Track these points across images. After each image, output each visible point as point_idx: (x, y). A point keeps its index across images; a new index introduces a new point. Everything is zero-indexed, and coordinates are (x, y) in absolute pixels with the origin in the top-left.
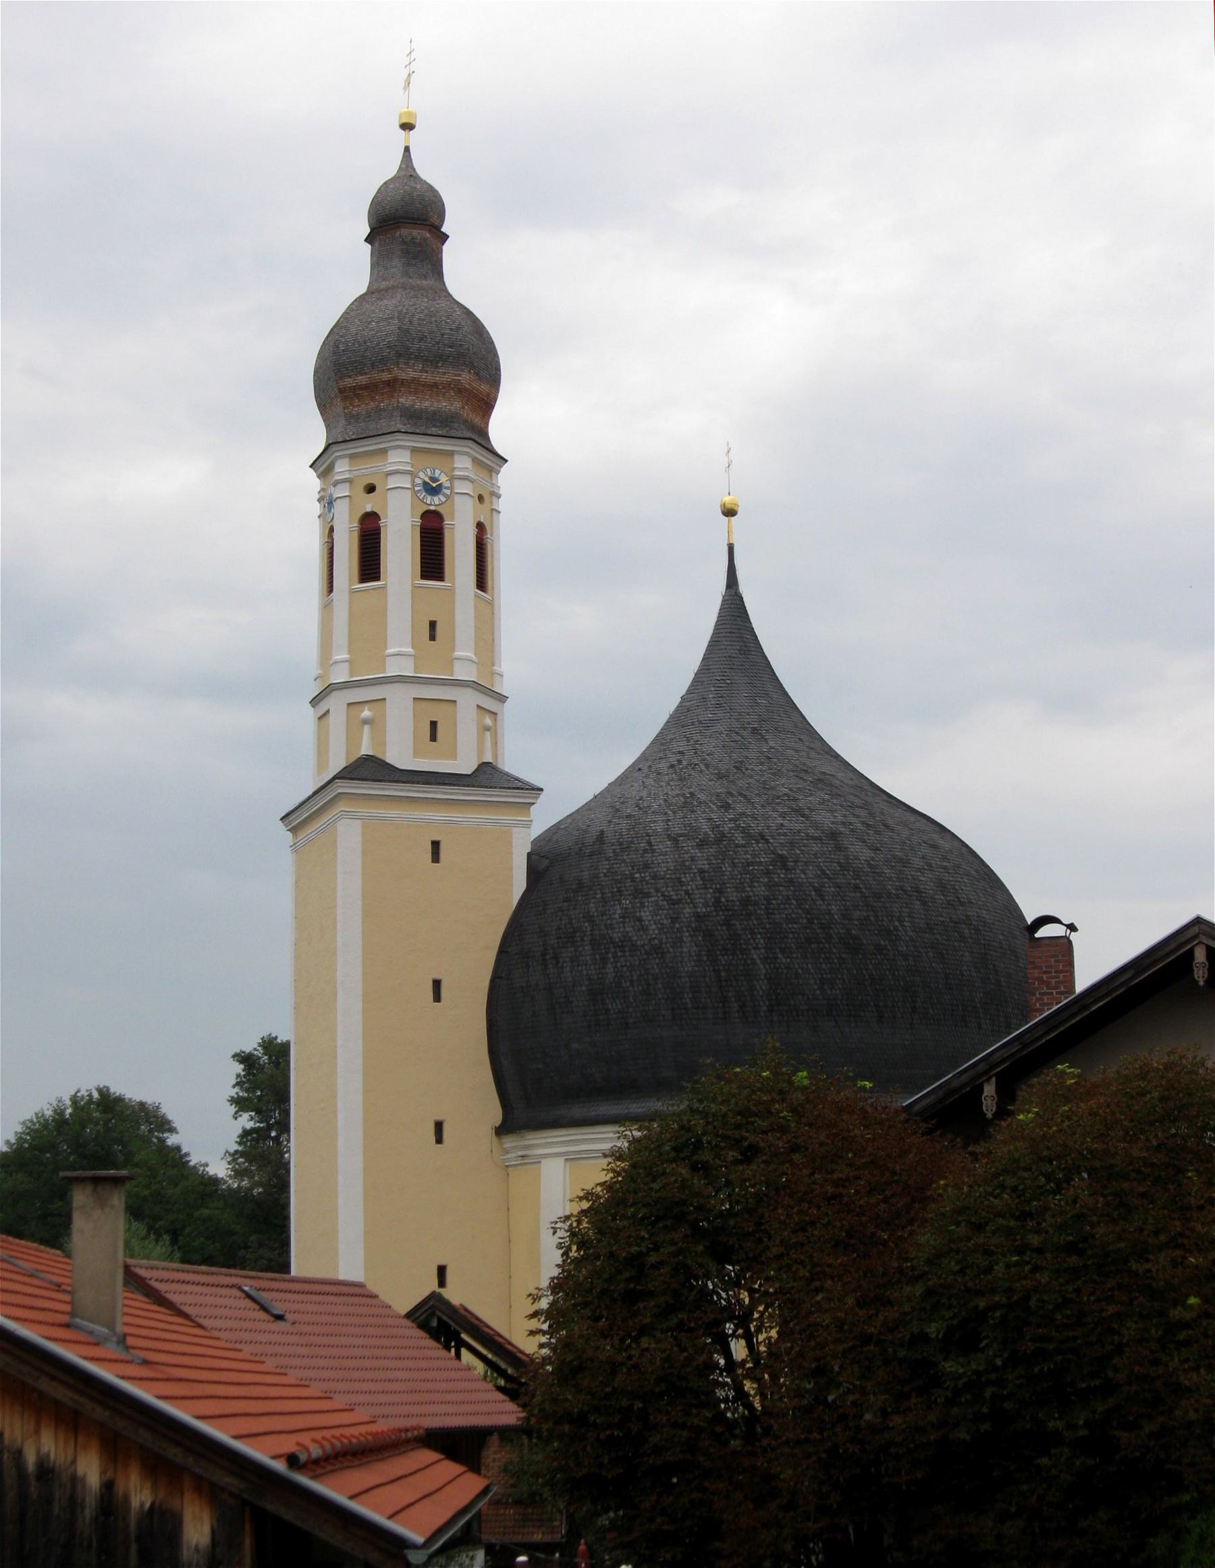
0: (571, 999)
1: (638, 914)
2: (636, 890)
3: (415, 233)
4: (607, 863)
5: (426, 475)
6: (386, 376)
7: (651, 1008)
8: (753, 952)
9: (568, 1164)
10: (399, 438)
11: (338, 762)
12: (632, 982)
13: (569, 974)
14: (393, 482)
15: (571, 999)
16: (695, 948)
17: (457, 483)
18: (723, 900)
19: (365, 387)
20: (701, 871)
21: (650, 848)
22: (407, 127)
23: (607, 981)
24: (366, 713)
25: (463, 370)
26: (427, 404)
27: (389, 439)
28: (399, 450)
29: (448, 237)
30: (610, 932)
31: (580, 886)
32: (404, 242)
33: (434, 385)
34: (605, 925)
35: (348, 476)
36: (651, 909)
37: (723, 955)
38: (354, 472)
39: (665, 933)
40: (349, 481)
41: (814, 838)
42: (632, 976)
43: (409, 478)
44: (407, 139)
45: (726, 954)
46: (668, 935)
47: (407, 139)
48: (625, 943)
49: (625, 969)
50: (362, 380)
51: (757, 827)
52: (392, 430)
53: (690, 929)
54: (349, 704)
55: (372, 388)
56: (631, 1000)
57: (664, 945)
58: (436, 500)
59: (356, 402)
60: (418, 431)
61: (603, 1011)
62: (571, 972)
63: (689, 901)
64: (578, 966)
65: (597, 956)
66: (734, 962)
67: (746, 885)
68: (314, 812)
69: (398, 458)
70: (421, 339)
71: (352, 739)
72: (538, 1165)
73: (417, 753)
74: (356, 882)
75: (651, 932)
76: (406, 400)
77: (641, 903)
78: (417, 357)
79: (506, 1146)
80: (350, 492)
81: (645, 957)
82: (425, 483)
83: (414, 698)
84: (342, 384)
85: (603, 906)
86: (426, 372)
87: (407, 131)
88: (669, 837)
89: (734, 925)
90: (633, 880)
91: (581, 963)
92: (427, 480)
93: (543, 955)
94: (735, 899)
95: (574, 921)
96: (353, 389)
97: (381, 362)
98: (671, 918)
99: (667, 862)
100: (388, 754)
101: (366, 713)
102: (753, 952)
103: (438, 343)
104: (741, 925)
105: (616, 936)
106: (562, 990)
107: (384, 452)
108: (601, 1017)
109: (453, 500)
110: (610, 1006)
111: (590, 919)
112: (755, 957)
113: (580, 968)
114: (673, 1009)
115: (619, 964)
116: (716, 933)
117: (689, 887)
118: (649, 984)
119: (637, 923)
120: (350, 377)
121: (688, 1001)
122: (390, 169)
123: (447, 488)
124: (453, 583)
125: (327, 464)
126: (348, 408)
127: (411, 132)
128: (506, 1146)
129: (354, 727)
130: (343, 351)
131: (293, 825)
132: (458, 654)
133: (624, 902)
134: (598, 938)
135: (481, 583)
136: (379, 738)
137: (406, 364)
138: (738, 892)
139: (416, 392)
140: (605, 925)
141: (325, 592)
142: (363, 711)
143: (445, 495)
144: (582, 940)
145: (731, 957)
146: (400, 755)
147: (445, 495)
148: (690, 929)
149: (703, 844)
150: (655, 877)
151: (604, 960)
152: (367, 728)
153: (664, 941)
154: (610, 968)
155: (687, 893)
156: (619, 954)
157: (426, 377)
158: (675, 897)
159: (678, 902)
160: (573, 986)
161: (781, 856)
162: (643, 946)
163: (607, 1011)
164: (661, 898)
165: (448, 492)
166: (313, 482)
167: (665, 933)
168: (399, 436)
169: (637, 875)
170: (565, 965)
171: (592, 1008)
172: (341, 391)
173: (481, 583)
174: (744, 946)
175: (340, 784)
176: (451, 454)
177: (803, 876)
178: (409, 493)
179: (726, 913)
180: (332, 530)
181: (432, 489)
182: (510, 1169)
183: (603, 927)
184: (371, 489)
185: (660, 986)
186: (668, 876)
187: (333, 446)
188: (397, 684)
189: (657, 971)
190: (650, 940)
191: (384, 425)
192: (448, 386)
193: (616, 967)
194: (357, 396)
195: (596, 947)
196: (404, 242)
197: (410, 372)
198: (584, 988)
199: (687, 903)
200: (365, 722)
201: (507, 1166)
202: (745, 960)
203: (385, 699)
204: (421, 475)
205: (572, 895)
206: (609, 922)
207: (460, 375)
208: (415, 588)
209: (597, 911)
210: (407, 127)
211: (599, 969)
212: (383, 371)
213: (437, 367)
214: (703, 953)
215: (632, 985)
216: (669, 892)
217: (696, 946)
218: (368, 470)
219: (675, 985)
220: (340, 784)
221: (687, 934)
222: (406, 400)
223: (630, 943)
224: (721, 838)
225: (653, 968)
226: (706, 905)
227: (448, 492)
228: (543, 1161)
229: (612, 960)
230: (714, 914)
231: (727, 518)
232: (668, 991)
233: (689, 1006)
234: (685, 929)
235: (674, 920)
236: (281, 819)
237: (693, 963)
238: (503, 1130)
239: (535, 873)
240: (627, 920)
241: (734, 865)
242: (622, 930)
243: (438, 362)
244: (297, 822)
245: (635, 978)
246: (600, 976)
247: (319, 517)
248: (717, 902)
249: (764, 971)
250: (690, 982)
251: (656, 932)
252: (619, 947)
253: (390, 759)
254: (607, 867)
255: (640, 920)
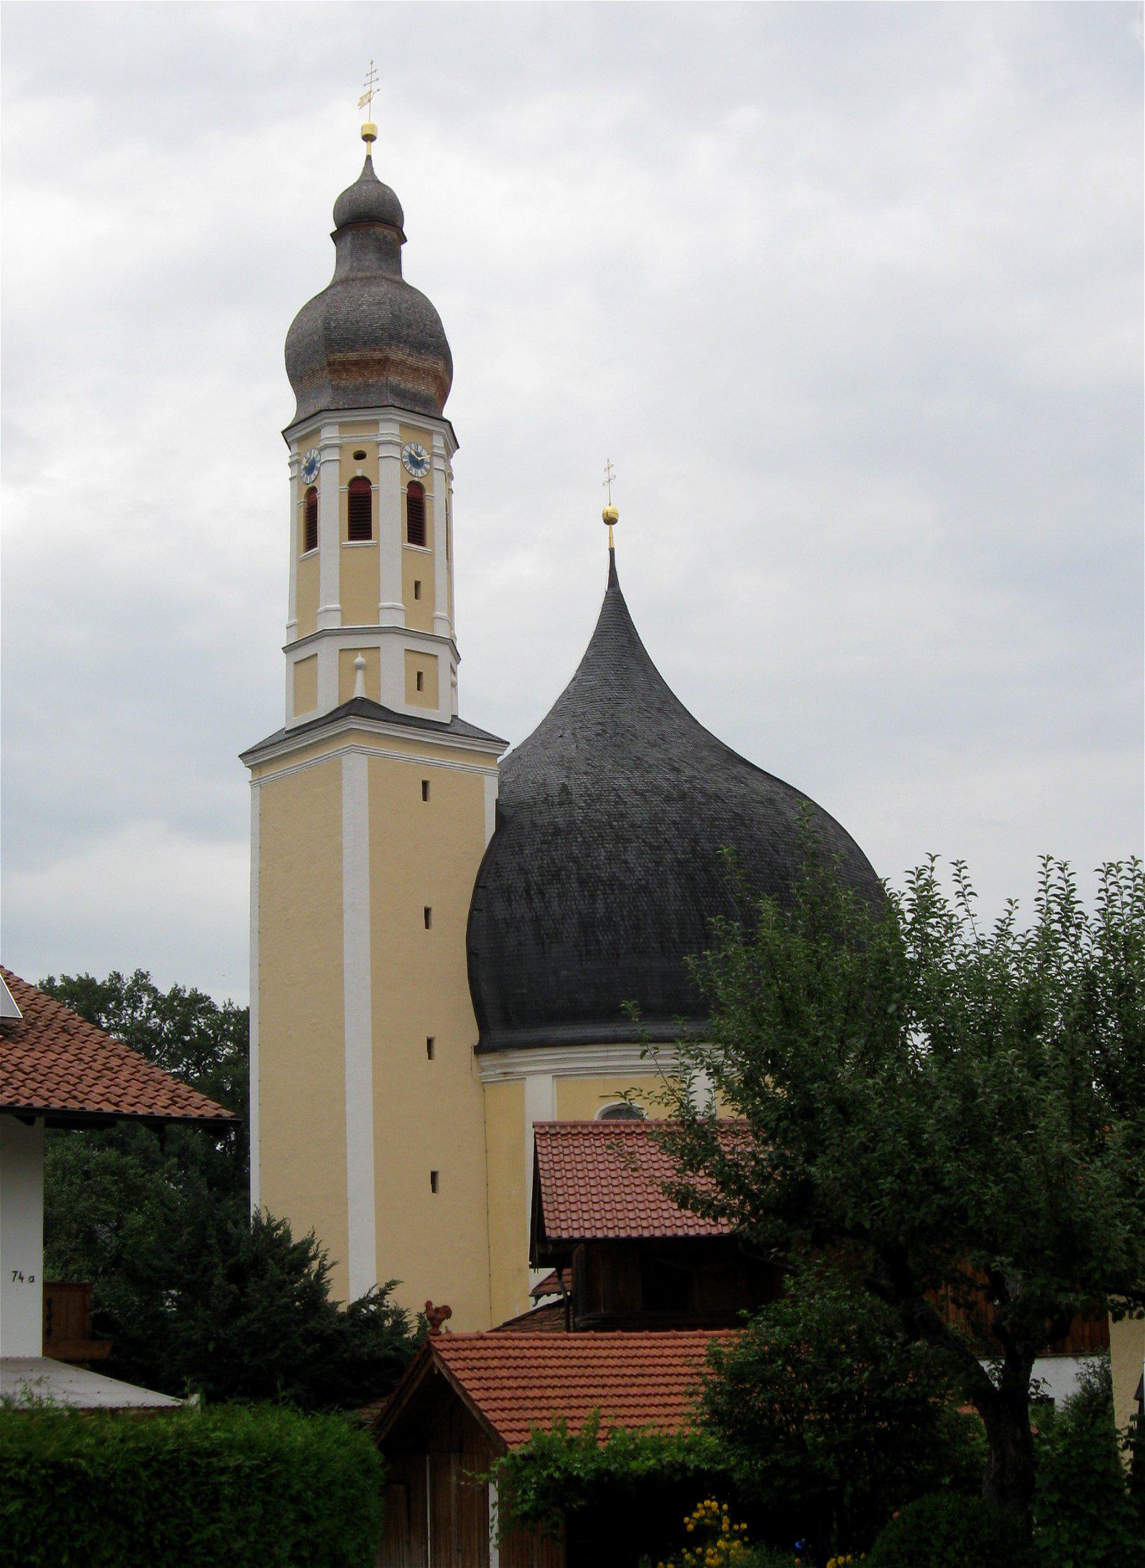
0: (560, 931)
1: (623, 857)
2: (617, 836)
3: (386, 232)
4: (580, 811)
5: (411, 448)
6: (377, 355)
7: (641, 941)
8: (729, 895)
9: (556, 1079)
10: (325, 416)
11: (327, 702)
12: (622, 917)
13: (557, 908)
14: (384, 451)
15: (560, 931)
16: (680, 890)
17: (435, 459)
18: (698, 849)
19: (355, 363)
20: (674, 823)
21: (620, 800)
22: (369, 138)
23: (598, 915)
24: (359, 659)
25: (440, 359)
26: (409, 385)
27: (346, 414)
28: (391, 423)
29: (458, 447)
30: (597, 871)
31: (557, 831)
32: (378, 240)
33: (416, 370)
34: (592, 865)
35: (338, 442)
36: (634, 853)
37: (704, 897)
38: (345, 439)
39: (652, 875)
40: (339, 446)
41: (758, 802)
42: (622, 911)
43: (398, 449)
44: (369, 149)
45: (707, 896)
46: (654, 877)
47: (369, 149)
48: (613, 882)
49: (615, 905)
50: (353, 356)
51: (711, 788)
52: (385, 403)
53: (673, 872)
54: (341, 650)
55: (362, 365)
56: (622, 932)
57: (651, 886)
58: (313, 477)
59: (344, 376)
60: (406, 408)
61: (595, 942)
62: (560, 906)
63: (669, 848)
64: (566, 901)
65: (586, 893)
66: (714, 904)
67: (716, 837)
68: (298, 749)
69: (389, 430)
70: (409, 326)
71: (345, 681)
72: (522, 1081)
73: (409, 700)
74: (364, 812)
75: (637, 873)
76: (394, 379)
77: (624, 847)
78: (405, 342)
79: (483, 1064)
80: (340, 456)
81: (634, 895)
82: (411, 456)
83: (406, 650)
84: (332, 358)
85: (586, 849)
86: (412, 356)
87: (369, 142)
88: (635, 791)
89: (710, 871)
90: (611, 827)
91: (569, 899)
92: (413, 453)
93: (527, 891)
94: (709, 849)
95: (556, 861)
96: (343, 364)
97: (373, 341)
98: (655, 862)
99: (641, 814)
100: (382, 698)
101: (359, 659)
102: (729, 895)
103: (422, 332)
104: (717, 871)
105: (604, 875)
106: (551, 922)
107: (375, 423)
108: (592, 948)
109: (433, 475)
110: (601, 938)
111: (575, 860)
112: (732, 900)
113: (569, 903)
114: (661, 942)
115: (608, 901)
116: (697, 877)
117: (666, 836)
118: (638, 920)
119: (623, 865)
120: (341, 352)
121: (675, 936)
122: (352, 176)
123: (427, 463)
124: (433, 549)
125: (314, 427)
126: (335, 380)
127: (373, 143)
128: (483, 1064)
129: (347, 672)
130: (335, 327)
131: (258, 762)
132: (382, 604)
133: (607, 845)
134: (585, 876)
135: (416, 531)
136: (371, 671)
137: (398, 347)
138: (710, 843)
139: (402, 374)
140: (592, 865)
141: (302, 547)
142: (356, 657)
143: (426, 469)
144: (569, 878)
145: (711, 899)
146: (394, 697)
147: (426, 469)
148: (673, 872)
149: (668, 799)
150: (632, 826)
151: (593, 897)
152: (360, 674)
153: (651, 881)
154: (600, 905)
155: (666, 841)
156: (608, 892)
157: (411, 361)
158: (656, 844)
159: (659, 848)
160: (562, 919)
161: (738, 815)
162: (631, 885)
163: (598, 942)
164: (642, 844)
165: (428, 466)
166: (283, 454)
167: (652, 875)
168: (393, 410)
169: (615, 823)
170: (552, 900)
171: (583, 939)
172: (330, 364)
173: (416, 531)
174: (721, 890)
175: (352, 720)
176: (430, 433)
177: (759, 833)
178: (398, 463)
179: (703, 860)
180: (312, 492)
181: (417, 464)
182: (486, 1085)
183: (589, 867)
184: (360, 456)
185: (650, 921)
186: (645, 826)
187: (323, 413)
188: (393, 635)
189: (646, 908)
190: (637, 881)
191: (373, 398)
192: (427, 372)
193: (606, 903)
194: (347, 370)
195: (584, 885)
196: (378, 240)
197: (397, 354)
198: (574, 921)
199: (667, 849)
200: (359, 667)
201: (484, 1083)
202: (724, 903)
203: (316, 655)
204: (407, 448)
205: (550, 838)
206: (595, 863)
207: (437, 364)
208: (405, 549)
209: (580, 853)
210: (369, 138)
211: (589, 904)
212: (375, 350)
213: (420, 353)
214: (687, 894)
215: (623, 920)
216: (649, 839)
217: (680, 887)
218: (359, 439)
219: (663, 921)
220: (352, 720)
221: (671, 877)
222: (394, 379)
223: (617, 882)
224: (683, 797)
225: (642, 905)
226: (684, 852)
227: (428, 466)
228: (529, 1079)
229: (601, 897)
230: (693, 860)
231: (608, 526)
232: (657, 925)
233: (677, 940)
234: (669, 872)
235: (658, 864)
236: (239, 756)
237: (678, 903)
238: (479, 1050)
239: (501, 820)
240: (613, 862)
241: (702, 820)
242: (609, 870)
243: (421, 349)
244: (263, 759)
245: (625, 913)
246: (590, 910)
247: (290, 479)
248: (694, 851)
249: (740, 913)
250: (677, 918)
251: (643, 873)
252: (608, 885)
253: (385, 702)
254: (582, 815)
255: (626, 862)
